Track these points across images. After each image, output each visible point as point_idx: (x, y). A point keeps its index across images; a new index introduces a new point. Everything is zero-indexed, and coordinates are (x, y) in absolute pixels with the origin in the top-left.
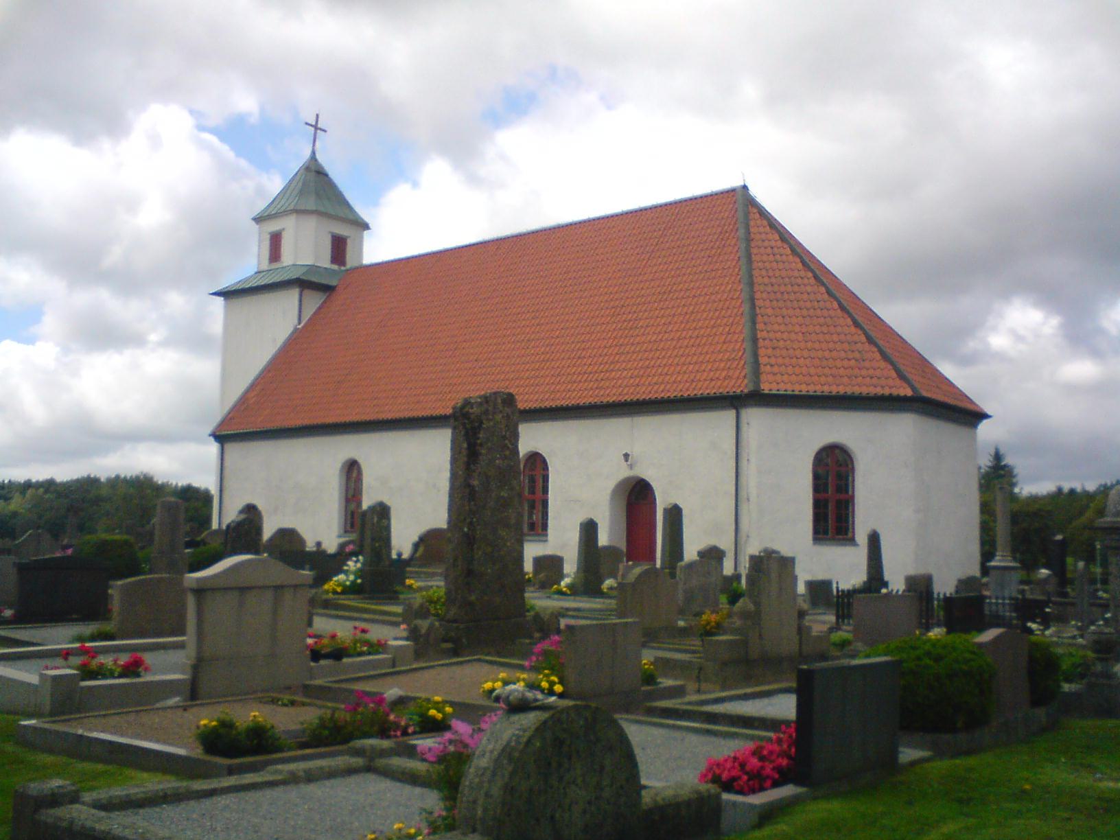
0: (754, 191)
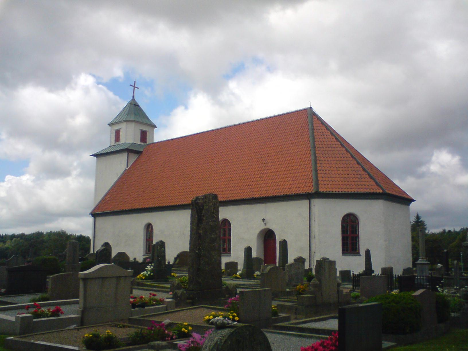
0: (315, 109)
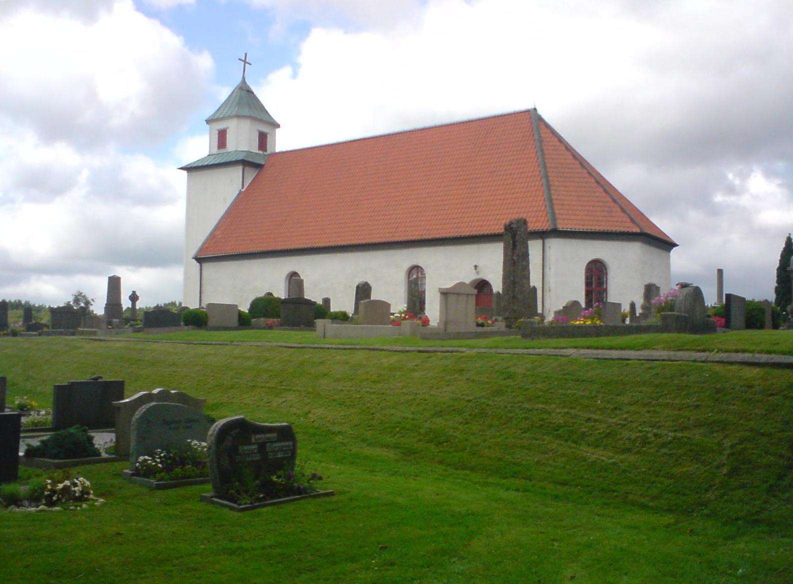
0: (542, 112)
